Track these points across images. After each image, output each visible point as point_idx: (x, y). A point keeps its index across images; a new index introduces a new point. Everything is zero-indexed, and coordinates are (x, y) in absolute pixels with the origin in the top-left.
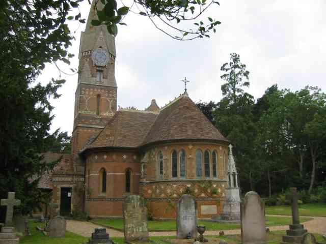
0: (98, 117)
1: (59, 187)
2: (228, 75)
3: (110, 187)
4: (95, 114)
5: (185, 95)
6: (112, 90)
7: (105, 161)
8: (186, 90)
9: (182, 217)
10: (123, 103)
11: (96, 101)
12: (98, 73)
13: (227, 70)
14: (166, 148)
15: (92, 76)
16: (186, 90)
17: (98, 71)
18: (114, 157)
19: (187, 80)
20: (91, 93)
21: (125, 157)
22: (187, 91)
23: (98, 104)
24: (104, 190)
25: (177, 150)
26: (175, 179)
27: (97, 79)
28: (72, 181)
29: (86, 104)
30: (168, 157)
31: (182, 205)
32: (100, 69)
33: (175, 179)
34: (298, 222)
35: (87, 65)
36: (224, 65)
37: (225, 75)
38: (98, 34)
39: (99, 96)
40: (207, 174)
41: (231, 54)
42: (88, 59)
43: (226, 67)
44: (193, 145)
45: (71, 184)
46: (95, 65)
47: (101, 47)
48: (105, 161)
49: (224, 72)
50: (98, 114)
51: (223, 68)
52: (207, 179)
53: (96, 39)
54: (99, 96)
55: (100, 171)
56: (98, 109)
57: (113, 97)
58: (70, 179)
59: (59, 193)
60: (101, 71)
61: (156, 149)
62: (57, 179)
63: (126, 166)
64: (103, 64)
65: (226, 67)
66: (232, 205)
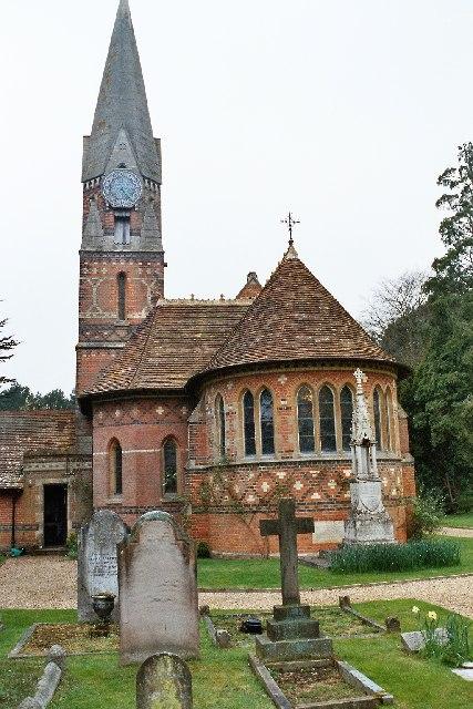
0: (123, 323)
1: (40, 483)
2: (457, 196)
3: (129, 484)
4: (115, 316)
5: (290, 256)
6: (153, 259)
7: (117, 424)
8: (291, 242)
9: (92, 568)
10: (179, 286)
11: (115, 291)
12: (120, 225)
13: (453, 185)
14: (230, 386)
15: (106, 234)
16: (291, 242)
17: (117, 219)
18: (135, 412)
19: (294, 218)
20: (104, 271)
21: (160, 411)
22: (294, 245)
23: (122, 295)
24: (119, 490)
25: (254, 391)
26: (307, 456)
27: (119, 238)
28: (68, 470)
29: (94, 296)
30: (234, 406)
31: (90, 540)
32: (124, 214)
33: (250, 459)
34: (296, 599)
35: (93, 208)
36: (448, 172)
37: (446, 198)
38: (114, 139)
39: (122, 276)
40: (329, 444)
41: (460, 148)
42: (96, 196)
43: (455, 177)
44: (286, 374)
45: (64, 476)
46: (110, 206)
47: (122, 166)
48: (118, 424)
49: (448, 191)
50: (122, 316)
51: (442, 180)
52: (329, 456)
53: (110, 148)
54: (122, 276)
55: (109, 446)
56: (122, 305)
57: (155, 275)
58: (61, 465)
59: (40, 498)
60: (126, 220)
61: (212, 390)
62: (34, 466)
63: (166, 430)
64: (126, 204)
65: (455, 177)
66: (358, 523)
